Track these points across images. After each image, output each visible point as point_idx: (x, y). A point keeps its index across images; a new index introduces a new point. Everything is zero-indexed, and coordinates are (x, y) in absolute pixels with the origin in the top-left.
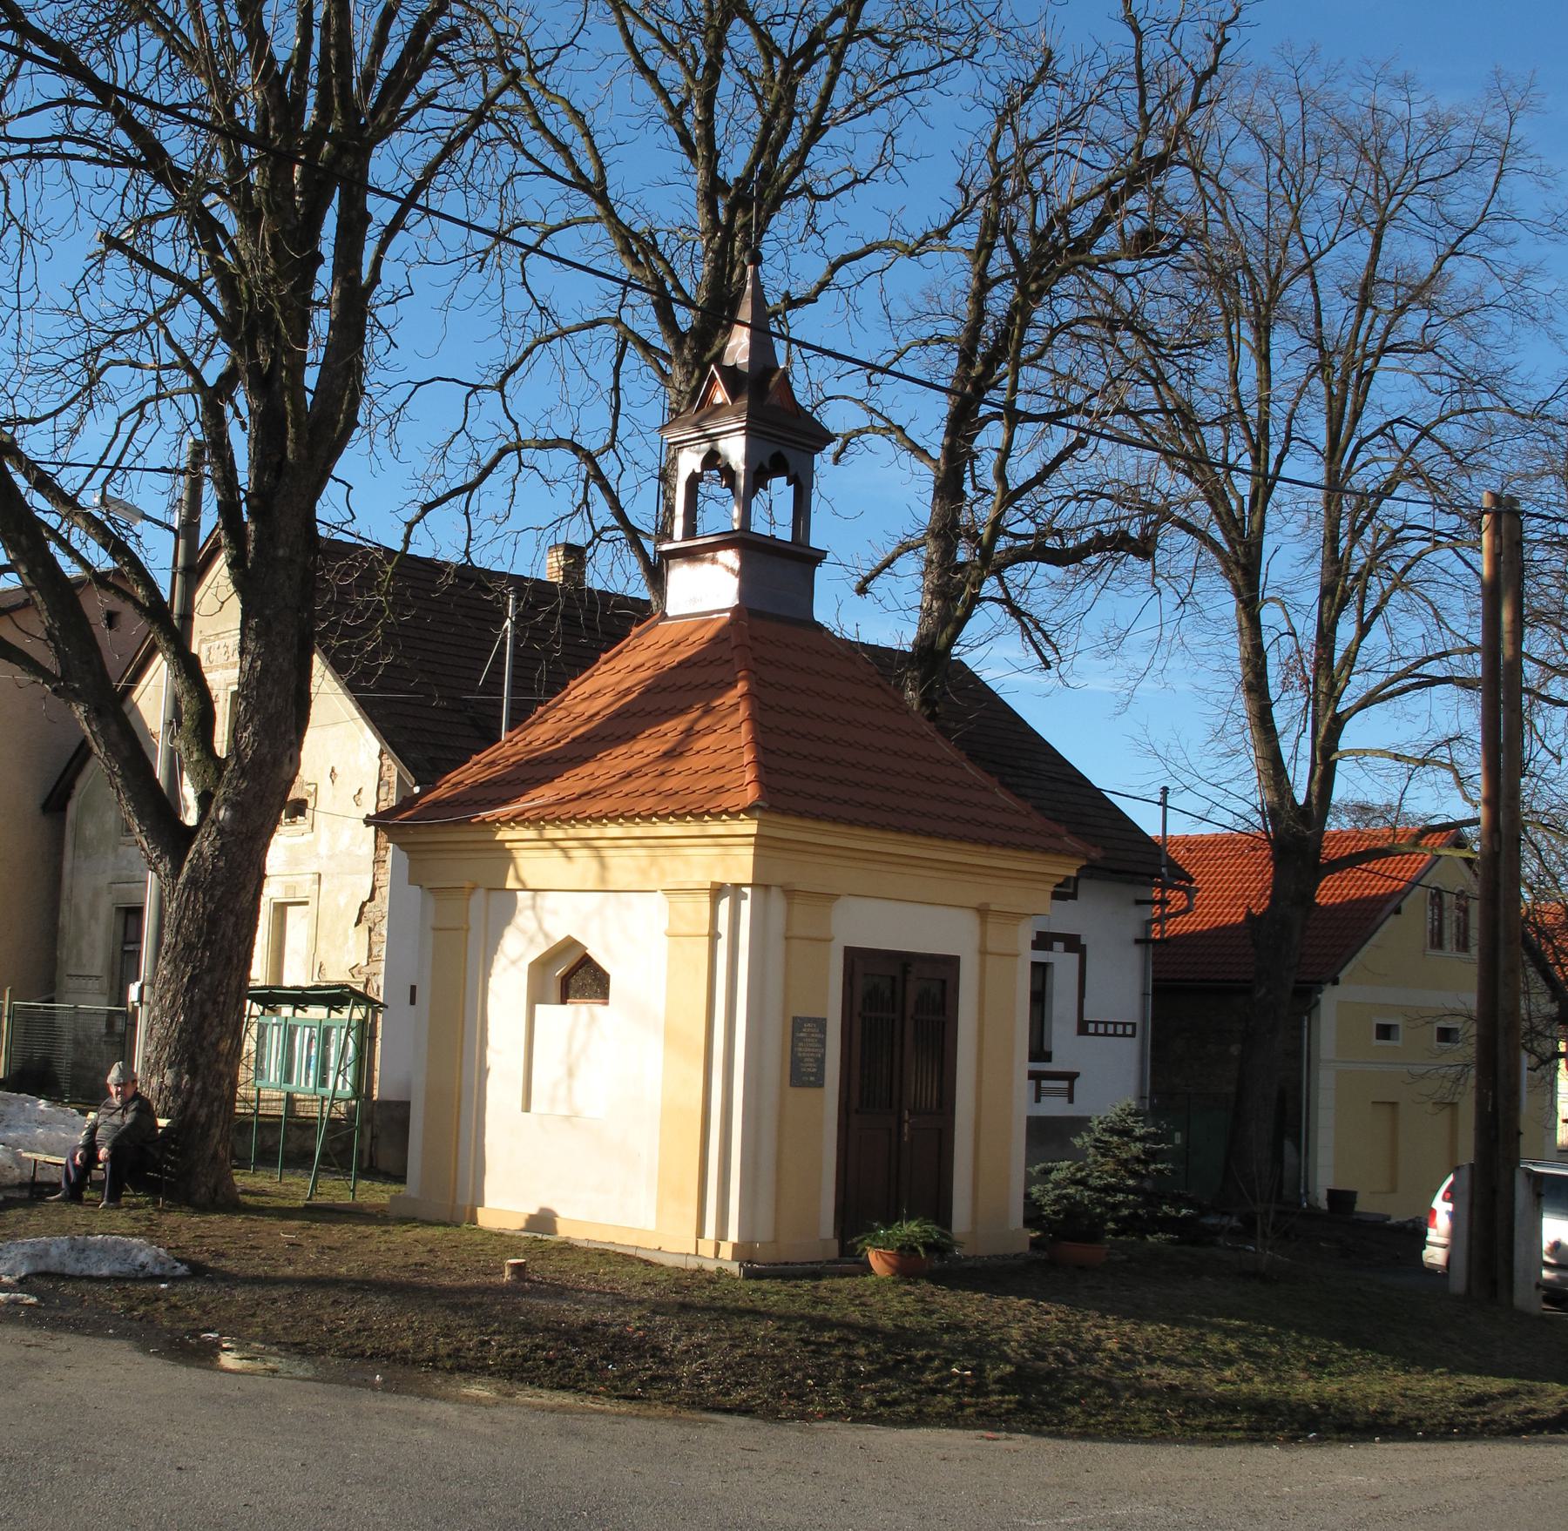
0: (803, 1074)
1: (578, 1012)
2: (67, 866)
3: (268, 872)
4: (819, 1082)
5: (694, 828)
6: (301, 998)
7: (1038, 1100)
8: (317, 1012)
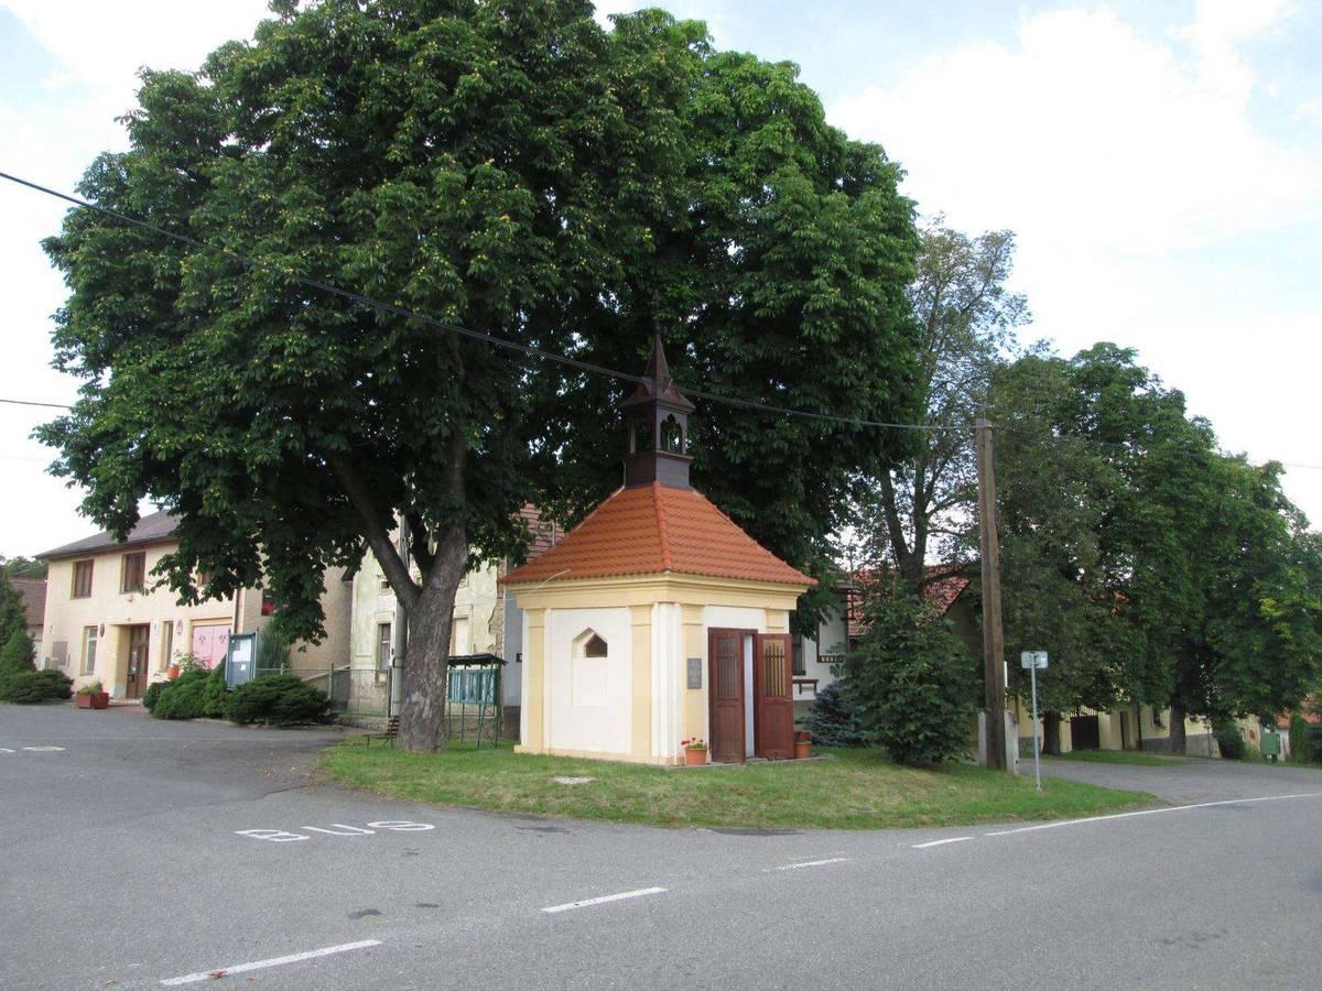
0: (693, 684)
1: (598, 660)
2: (354, 605)
3: (456, 604)
4: (699, 686)
5: (533, 824)
6: (467, 661)
7: (800, 692)
8: (475, 667)
